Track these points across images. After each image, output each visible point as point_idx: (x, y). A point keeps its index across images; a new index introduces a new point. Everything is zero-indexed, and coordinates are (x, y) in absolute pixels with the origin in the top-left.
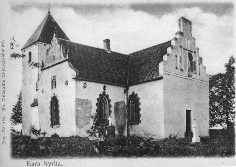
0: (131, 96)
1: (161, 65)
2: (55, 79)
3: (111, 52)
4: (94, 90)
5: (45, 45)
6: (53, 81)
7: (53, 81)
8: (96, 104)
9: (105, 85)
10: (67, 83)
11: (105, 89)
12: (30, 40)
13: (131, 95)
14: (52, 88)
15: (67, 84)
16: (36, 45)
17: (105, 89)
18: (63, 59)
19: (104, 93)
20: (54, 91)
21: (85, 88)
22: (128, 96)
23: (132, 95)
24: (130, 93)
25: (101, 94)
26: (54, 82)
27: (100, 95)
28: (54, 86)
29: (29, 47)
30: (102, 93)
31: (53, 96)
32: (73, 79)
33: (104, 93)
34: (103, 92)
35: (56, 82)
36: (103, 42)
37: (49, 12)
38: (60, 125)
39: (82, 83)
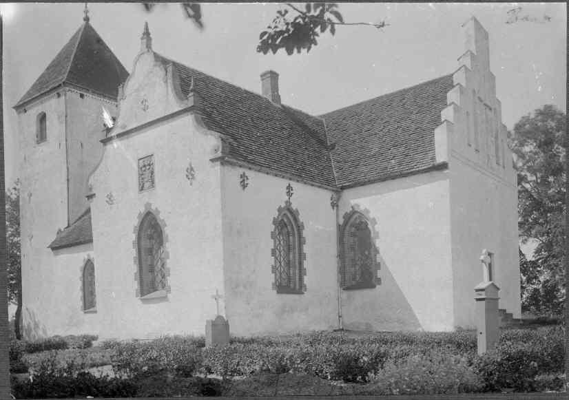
0: (348, 217)
1: (440, 135)
2: (149, 165)
3: (283, 106)
4: (269, 191)
5: (82, 96)
6: (144, 169)
7: (144, 169)
8: (272, 235)
9: (289, 185)
10: (190, 173)
11: (289, 194)
12: (41, 82)
13: (348, 212)
14: (142, 189)
15: (193, 175)
16: (59, 95)
17: (289, 194)
18: (177, 108)
19: (288, 203)
20: (146, 196)
21: (244, 188)
22: (342, 213)
23: (351, 212)
24: (345, 209)
25: (282, 206)
26: (147, 174)
27: (280, 210)
28: (147, 185)
29: (40, 100)
30: (283, 205)
31: (143, 210)
32: (212, 160)
33: (288, 203)
34: (286, 202)
35: (152, 173)
36: (260, 78)
37: (87, 19)
38: (169, 291)
39: (234, 174)
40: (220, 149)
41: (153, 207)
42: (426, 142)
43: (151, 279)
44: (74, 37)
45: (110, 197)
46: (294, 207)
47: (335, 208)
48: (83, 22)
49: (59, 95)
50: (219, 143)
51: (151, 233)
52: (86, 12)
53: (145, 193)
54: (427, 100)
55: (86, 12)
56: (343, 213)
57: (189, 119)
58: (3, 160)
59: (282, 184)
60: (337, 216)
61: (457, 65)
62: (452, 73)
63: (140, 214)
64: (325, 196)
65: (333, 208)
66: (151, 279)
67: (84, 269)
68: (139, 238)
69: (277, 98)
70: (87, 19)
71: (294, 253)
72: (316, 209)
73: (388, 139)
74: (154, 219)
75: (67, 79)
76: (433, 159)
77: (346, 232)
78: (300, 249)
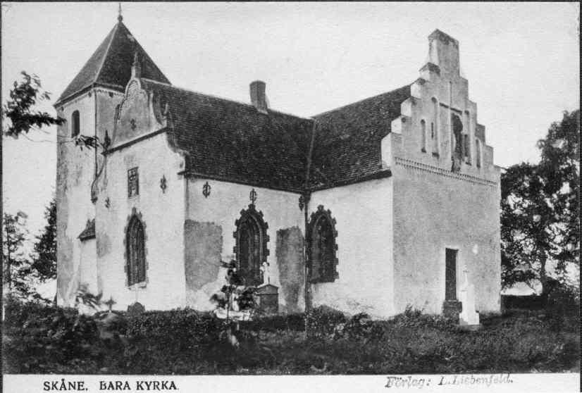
3: (269, 111)
4: (226, 201)
14: (130, 195)
16: (90, 95)
19: (252, 207)
26: (134, 182)
28: (134, 192)
33: (252, 207)
37: (120, 18)
38: (148, 282)
42: (375, 153)
43: (136, 272)
44: (107, 40)
45: (108, 201)
46: (258, 209)
48: (117, 22)
52: (120, 7)
53: (133, 198)
55: (120, 7)
57: (163, 138)
59: (247, 189)
60: (306, 214)
62: (408, 84)
64: (295, 198)
66: (136, 272)
67: (144, 267)
68: (128, 237)
69: (265, 106)
70: (120, 18)
73: (332, 150)
74: (138, 221)
76: (381, 167)
77: (314, 230)
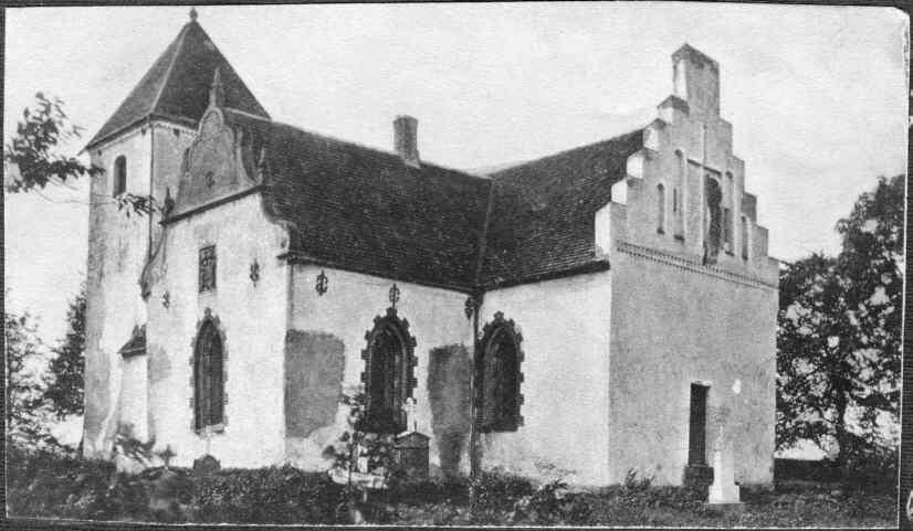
0: (489, 329)
4: (352, 304)
5: (177, 132)
10: (255, 273)
19: (392, 311)
24: (487, 317)
26: (208, 268)
33: (392, 311)
38: (226, 424)
40: (288, 243)
41: (213, 314)
45: (167, 297)
46: (401, 315)
47: (472, 318)
49: (144, 132)
50: (286, 235)
51: (210, 344)
54: (597, 169)
56: (484, 324)
58: (135, 4)
61: (654, 115)
63: (199, 323)
64: (459, 300)
65: (469, 317)
71: (204, 388)
72: (437, 319)
75: (156, 109)
78: (410, 372)
